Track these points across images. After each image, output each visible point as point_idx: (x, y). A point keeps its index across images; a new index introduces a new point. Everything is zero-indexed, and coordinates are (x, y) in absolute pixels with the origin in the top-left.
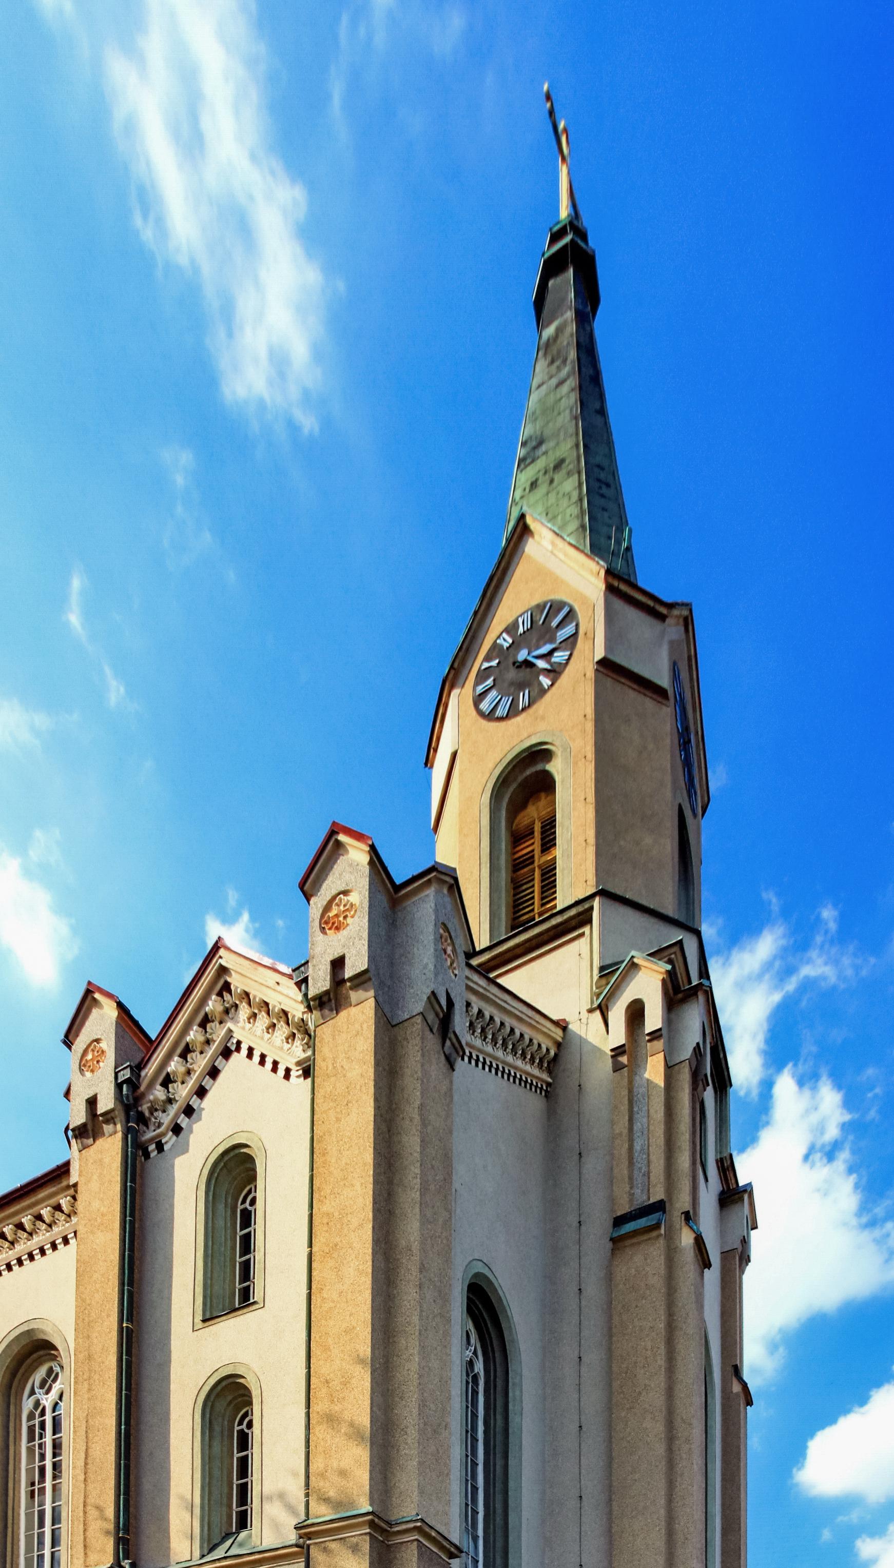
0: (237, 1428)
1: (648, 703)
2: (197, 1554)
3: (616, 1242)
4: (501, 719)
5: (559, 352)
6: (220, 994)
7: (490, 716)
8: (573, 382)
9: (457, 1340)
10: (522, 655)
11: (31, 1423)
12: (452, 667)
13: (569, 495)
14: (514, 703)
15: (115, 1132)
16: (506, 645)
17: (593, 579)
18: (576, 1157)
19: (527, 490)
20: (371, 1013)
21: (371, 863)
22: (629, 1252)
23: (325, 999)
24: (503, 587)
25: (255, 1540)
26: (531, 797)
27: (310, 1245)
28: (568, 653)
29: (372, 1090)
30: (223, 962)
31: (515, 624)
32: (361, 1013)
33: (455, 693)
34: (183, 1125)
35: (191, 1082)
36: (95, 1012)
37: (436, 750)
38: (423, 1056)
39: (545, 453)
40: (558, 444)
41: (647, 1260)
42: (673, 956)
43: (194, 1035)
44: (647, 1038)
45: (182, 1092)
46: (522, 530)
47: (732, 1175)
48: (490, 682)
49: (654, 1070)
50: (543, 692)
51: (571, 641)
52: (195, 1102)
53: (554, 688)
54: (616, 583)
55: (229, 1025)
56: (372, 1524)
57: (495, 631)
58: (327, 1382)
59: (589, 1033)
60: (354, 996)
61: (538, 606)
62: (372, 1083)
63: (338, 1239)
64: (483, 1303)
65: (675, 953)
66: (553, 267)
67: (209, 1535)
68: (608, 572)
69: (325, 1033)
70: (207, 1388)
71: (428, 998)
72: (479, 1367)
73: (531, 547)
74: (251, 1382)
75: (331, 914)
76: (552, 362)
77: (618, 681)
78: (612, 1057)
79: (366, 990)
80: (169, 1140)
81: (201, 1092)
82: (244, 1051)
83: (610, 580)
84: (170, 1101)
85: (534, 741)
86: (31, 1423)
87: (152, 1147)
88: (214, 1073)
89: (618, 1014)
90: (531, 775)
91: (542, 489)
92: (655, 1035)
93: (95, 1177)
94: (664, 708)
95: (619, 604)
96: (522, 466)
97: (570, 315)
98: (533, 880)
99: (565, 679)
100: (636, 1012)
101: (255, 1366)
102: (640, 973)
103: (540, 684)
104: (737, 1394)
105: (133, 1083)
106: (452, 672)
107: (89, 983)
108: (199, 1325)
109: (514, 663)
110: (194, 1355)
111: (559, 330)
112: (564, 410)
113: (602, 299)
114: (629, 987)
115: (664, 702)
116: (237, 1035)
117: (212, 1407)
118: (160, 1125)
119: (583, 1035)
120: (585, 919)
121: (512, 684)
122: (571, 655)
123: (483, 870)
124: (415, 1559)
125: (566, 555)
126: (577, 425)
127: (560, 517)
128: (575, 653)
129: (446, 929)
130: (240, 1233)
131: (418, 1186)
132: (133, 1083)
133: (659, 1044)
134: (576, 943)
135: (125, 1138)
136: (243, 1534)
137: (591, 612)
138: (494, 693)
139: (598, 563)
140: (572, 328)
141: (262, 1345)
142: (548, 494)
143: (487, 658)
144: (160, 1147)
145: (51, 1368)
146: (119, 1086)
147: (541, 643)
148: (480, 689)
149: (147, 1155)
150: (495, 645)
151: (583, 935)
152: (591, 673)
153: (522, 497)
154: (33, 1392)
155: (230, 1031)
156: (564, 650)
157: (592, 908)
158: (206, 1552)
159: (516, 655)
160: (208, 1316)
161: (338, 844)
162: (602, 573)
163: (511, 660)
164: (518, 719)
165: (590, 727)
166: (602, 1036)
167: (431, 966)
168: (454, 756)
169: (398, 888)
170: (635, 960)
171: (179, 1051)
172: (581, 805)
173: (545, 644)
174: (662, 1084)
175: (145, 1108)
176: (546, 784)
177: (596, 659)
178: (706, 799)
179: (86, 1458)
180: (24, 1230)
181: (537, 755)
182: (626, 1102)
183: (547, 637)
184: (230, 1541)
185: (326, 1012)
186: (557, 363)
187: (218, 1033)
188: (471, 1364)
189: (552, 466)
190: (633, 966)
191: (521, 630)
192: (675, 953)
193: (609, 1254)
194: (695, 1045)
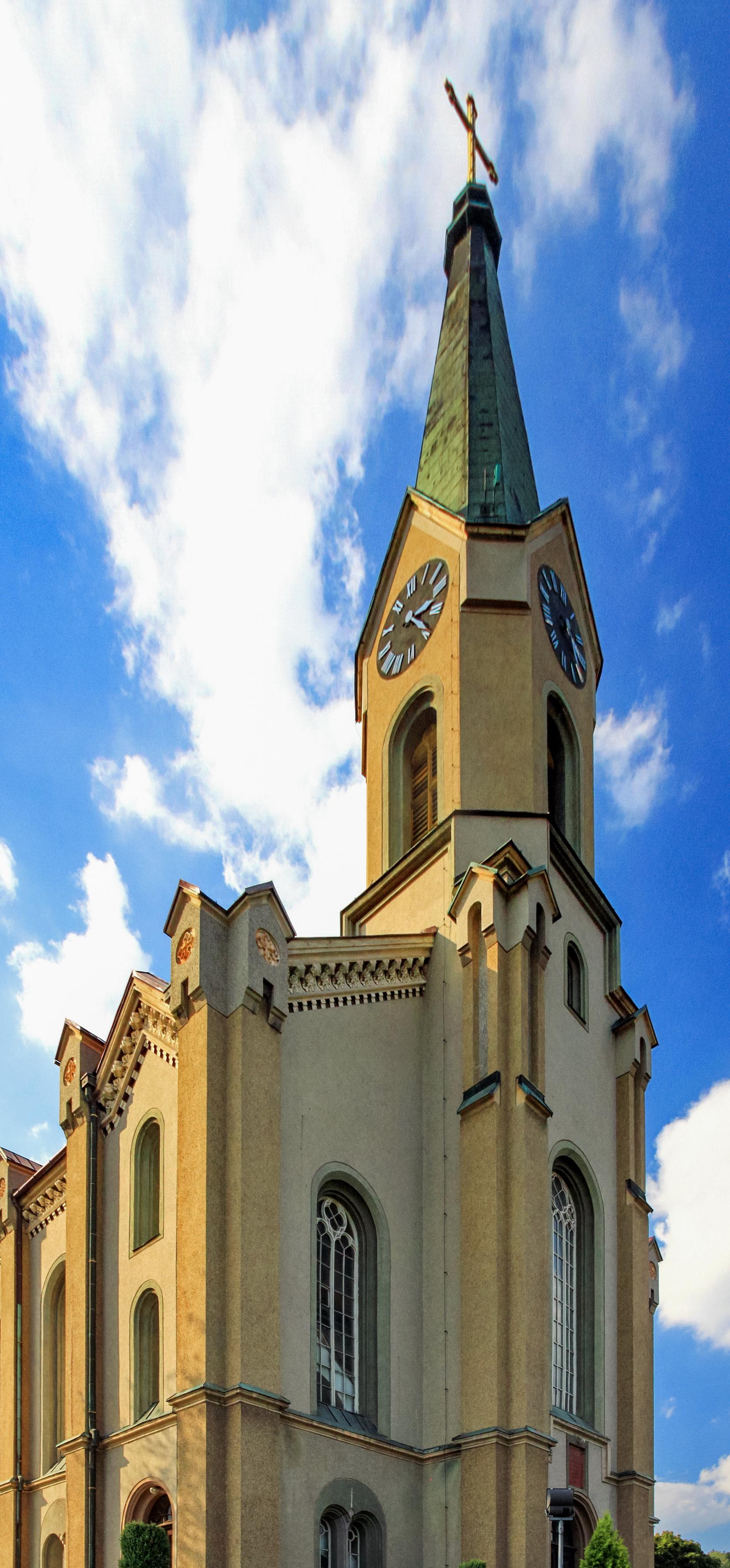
1: (513, 621)
2: (132, 1421)
4: (397, 675)
7: (388, 676)
8: (465, 342)
10: (409, 617)
12: (361, 642)
13: (456, 450)
15: (83, 1122)
17: (458, 532)
18: (442, 1043)
19: (331, 552)
23: (180, 1011)
24: (397, 559)
26: (423, 732)
28: (441, 604)
31: (405, 591)
33: (366, 661)
34: (124, 1108)
36: (71, 1039)
40: (452, 403)
41: (487, 1123)
42: (507, 855)
43: (125, 1043)
44: (484, 934)
45: (121, 1083)
46: (409, 506)
47: (628, 1003)
48: (388, 646)
49: (492, 960)
50: (425, 642)
52: (129, 1090)
53: (432, 638)
54: (475, 530)
55: (143, 1031)
56: (208, 1396)
59: (452, 935)
64: (341, 1193)
65: (509, 852)
67: (141, 1406)
68: (468, 525)
70: (136, 1300)
71: (246, 992)
73: (416, 520)
74: (157, 1292)
75: (182, 948)
77: (484, 613)
78: (460, 955)
79: (202, 1000)
80: (116, 1119)
81: (132, 1082)
82: (153, 1049)
83: (470, 529)
84: (116, 1092)
85: (418, 688)
87: (108, 1127)
88: (138, 1067)
89: (463, 916)
90: (421, 715)
92: (490, 930)
94: (526, 617)
101: (159, 1281)
102: (478, 880)
104: (630, 1206)
105: (91, 1086)
106: (362, 646)
108: (132, 1254)
109: (404, 625)
110: (132, 1272)
114: (473, 890)
116: (149, 1038)
117: (141, 1312)
119: (447, 937)
124: (240, 1417)
125: (439, 518)
131: (240, 1138)
132: (91, 1086)
133: (493, 937)
135: (89, 1126)
138: (391, 654)
139: (459, 520)
143: (386, 627)
144: (112, 1125)
146: (83, 1089)
148: (381, 654)
149: (106, 1132)
150: (392, 612)
157: (450, 828)
160: (138, 1246)
162: (463, 526)
165: (456, 663)
166: (458, 934)
167: (247, 968)
169: (227, 913)
170: (473, 870)
171: (117, 1057)
174: (496, 971)
175: (101, 1101)
176: (431, 717)
177: (461, 603)
178: (599, 661)
181: (423, 697)
182: (472, 992)
185: (182, 1019)
187: (138, 1037)
190: (473, 875)
192: (509, 852)
194: (525, 928)
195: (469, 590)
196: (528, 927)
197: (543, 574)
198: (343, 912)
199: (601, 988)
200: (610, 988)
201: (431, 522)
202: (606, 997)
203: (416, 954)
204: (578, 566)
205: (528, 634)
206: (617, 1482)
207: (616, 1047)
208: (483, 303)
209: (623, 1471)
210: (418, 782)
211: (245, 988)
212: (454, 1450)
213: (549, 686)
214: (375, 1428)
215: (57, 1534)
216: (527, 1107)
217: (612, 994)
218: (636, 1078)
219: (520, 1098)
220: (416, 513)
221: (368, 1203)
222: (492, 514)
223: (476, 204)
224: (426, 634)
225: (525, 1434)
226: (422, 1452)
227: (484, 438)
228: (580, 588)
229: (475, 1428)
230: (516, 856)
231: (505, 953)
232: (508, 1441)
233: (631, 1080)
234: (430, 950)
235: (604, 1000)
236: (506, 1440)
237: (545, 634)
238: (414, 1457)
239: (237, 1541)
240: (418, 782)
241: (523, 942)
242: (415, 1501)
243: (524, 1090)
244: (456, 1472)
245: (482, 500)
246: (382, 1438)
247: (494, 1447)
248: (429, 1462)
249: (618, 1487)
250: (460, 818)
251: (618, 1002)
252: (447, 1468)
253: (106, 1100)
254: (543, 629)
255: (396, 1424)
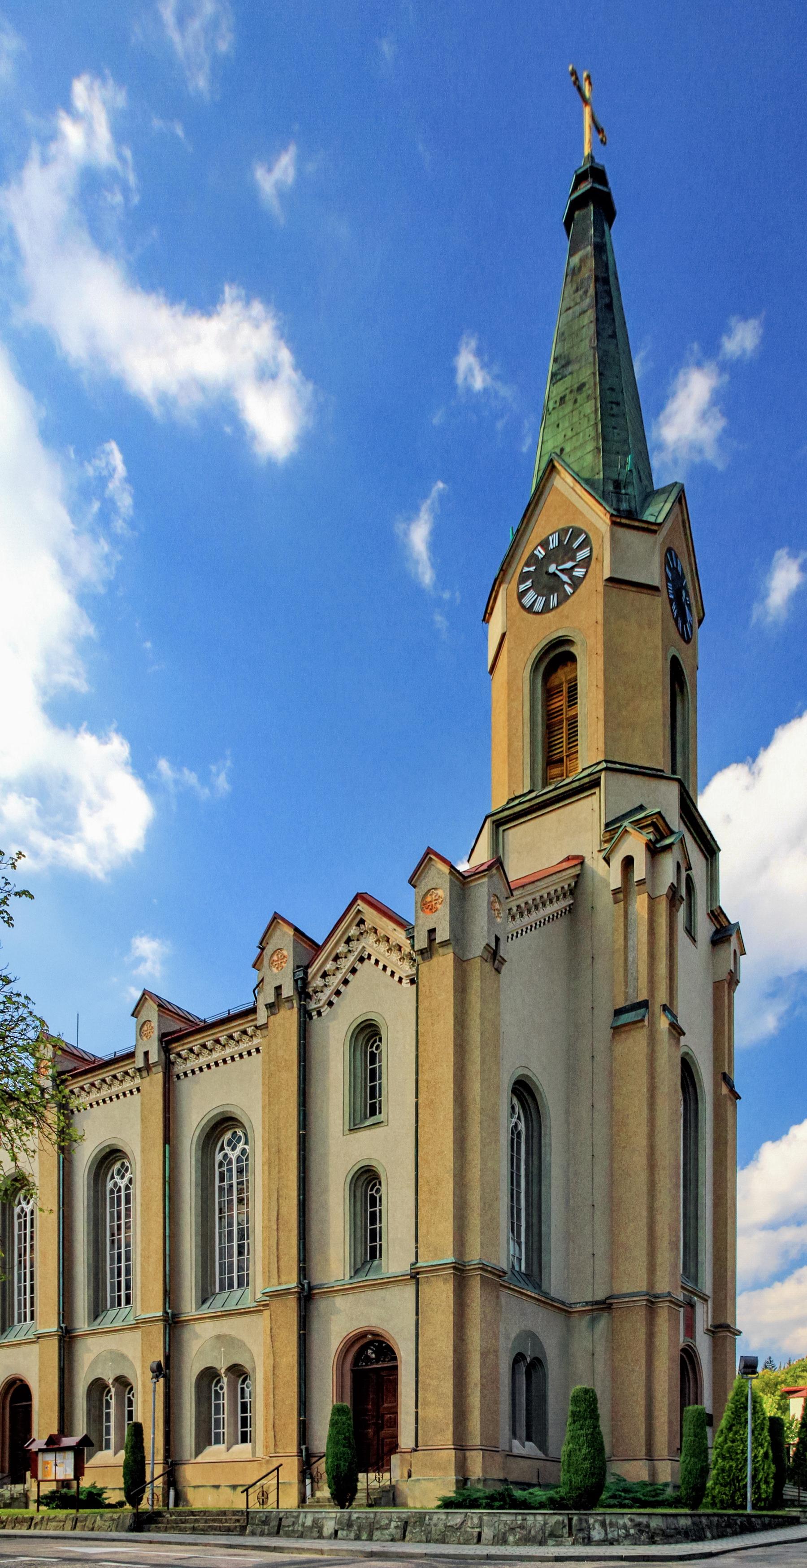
0: (369, 1193)
1: (645, 598)
2: (347, 1277)
3: (616, 1030)
4: (537, 613)
5: (582, 283)
6: (358, 925)
7: (530, 610)
8: (591, 315)
9: (505, 1109)
10: (552, 568)
11: (222, 1169)
12: (501, 570)
14: (547, 602)
16: (541, 556)
20: (451, 963)
21: (451, 873)
22: (623, 1036)
25: (384, 1269)
27: (417, 1097)
29: (452, 1010)
30: (359, 908)
32: (444, 961)
35: (340, 976)
37: (491, 614)
38: (482, 981)
39: (571, 373)
41: (635, 1044)
45: (334, 981)
49: (640, 904)
50: (567, 597)
51: (586, 563)
56: (454, 1268)
57: (532, 546)
58: (428, 1182)
60: (441, 950)
61: (563, 530)
62: (452, 1006)
63: (433, 1097)
64: (524, 1091)
66: (577, 204)
69: (424, 967)
70: (352, 1172)
72: (522, 1126)
76: (577, 290)
80: (325, 1010)
82: (373, 961)
83: (614, 519)
86: (222, 1169)
88: (354, 971)
91: (569, 407)
92: (641, 882)
93: (280, 1035)
95: (621, 531)
96: (554, 380)
97: (589, 249)
98: (562, 728)
99: (582, 589)
100: (628, 862)
103: (565, 590)
104: (725, 1095)
107: (275, 913)
108: (348, 1132)
111: (582, 261)
112: (586, 338)
113: (618, 213)
115: (657, 594)
118: (319, 1000)
120: (596, 783)
121: (545, 587)
122: (586, 572)
123: (525, 729)
124: (479, 1285)
126: (594, 356)
127: (581, 434)
128: (590, 570)
129: (495, 895)
130: (369, 1067)
134: (590, 799)
136: (376, 1262)
137: (601, 540)
140: (591, 263)
141: (386, 1146)
142: (572, 411)
144: (319, 1014)
145: (235, 1132)
146: (296, 981)
147: (566, 558)
149: (311, 1018)
150: (533, 555)
151: (595, 793)
152: (601, 588)
153: (554, 408)
154: (222, 1149)
155: (364, 947)
156: (581, 568)
157: (600, 778)
158: (353, 1274)
159: (548, 568)
161: (431, 859)
163: (545, 570)
164: (549, 615)
167: (486, 928)
168: (503, 636)
172: (594, 688)
173: (568, 561)
175: (310, 990)
179: (278, 1215)
180: (220, 1044)
183: (570, 555)
184: (368, 1267)
186: (581, 292)
187: (357, 946)
188: (516, 1126)
189: (576, 386)
191: (551, 547)
193: (610, 1036)
195: (612, 570)
196: (672, 884)
197: (670, 556)
198: (487, 817)
199: (704, 906)
200: (711, 906)
201: (573, 493)
202: (708, 914)
203: (569, 882)
204: (688, 532)
205: (658, 607)
206: (713, 1332)
207: (713, 952)
208: (606, 281)
209: (718, 1323)
210: (553, 707)
211: (484, 944)
212: (605, 1306)
213: (673, 651)
214: (540, 1286)
215: (217, 1366)
216: (669, 1030)
217: (712, 912)
218: (730, 984)
219: (664, 1023)
220: (558, 477)
221: (538, 1097)
222: (623, 491)
223: (597, 186)
224: (569, 590)
225: (669, 1298)
226: (570, 1305)
227: (613, 415)
228: (689, 555)
229: (625, 1290)
230: (661, 821)
231: (652, 900)
232: (652, 1302)
233: (726, 986)
234: (578, 876)
235: (706, 916)
236: (652, 1302)
237: (668, 606)
238: (564, 1310)
239: (476, 1384)
240: (553, 707)
241: (667, 895)
242: (565, 1347)
243: (667, 1016)
244: (602, 1324)
245: (616, 477)
246: (546, 1294)
247: (643, 1308)
248: (576, 1315)
249: (713, 1337)
250: (609, 773)
251: (716, 917)
252: (593, 1321)
253: (316, 992)
254: (668, 601)
255: (555, 1282)
